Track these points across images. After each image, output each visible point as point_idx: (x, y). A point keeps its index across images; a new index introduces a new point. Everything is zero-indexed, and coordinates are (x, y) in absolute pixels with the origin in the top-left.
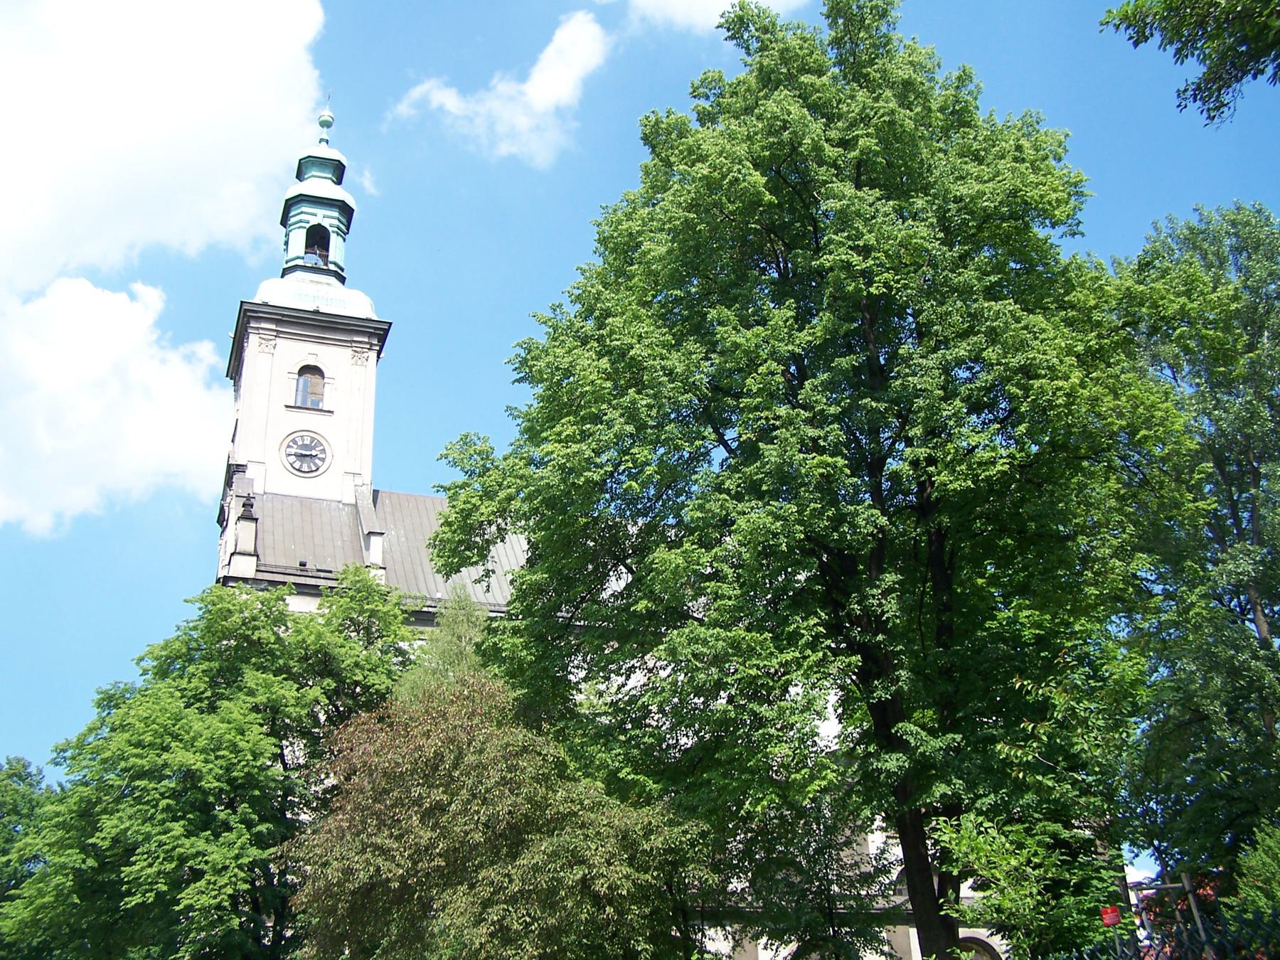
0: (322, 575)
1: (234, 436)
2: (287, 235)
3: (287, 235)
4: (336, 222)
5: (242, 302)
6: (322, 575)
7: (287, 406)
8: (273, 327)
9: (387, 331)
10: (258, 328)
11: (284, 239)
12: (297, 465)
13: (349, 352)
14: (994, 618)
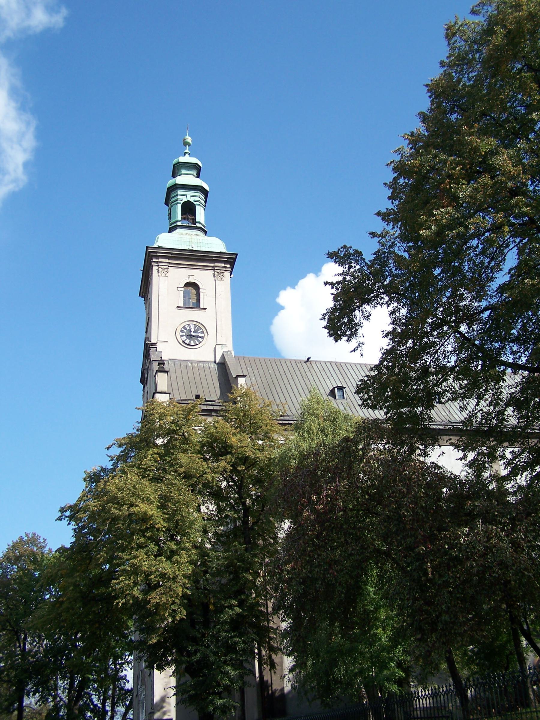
0: (210, 403)
1: (147, 329)
2: (170, 210)
3: (170, 210)
5: (147, 247)
6: (210, 403)
7: (178, 307)
8: (167, 261)
9: (235, 259)
10: (157, 262)
11: (167, 213)
12: (187, 341)
14: (429, 366)
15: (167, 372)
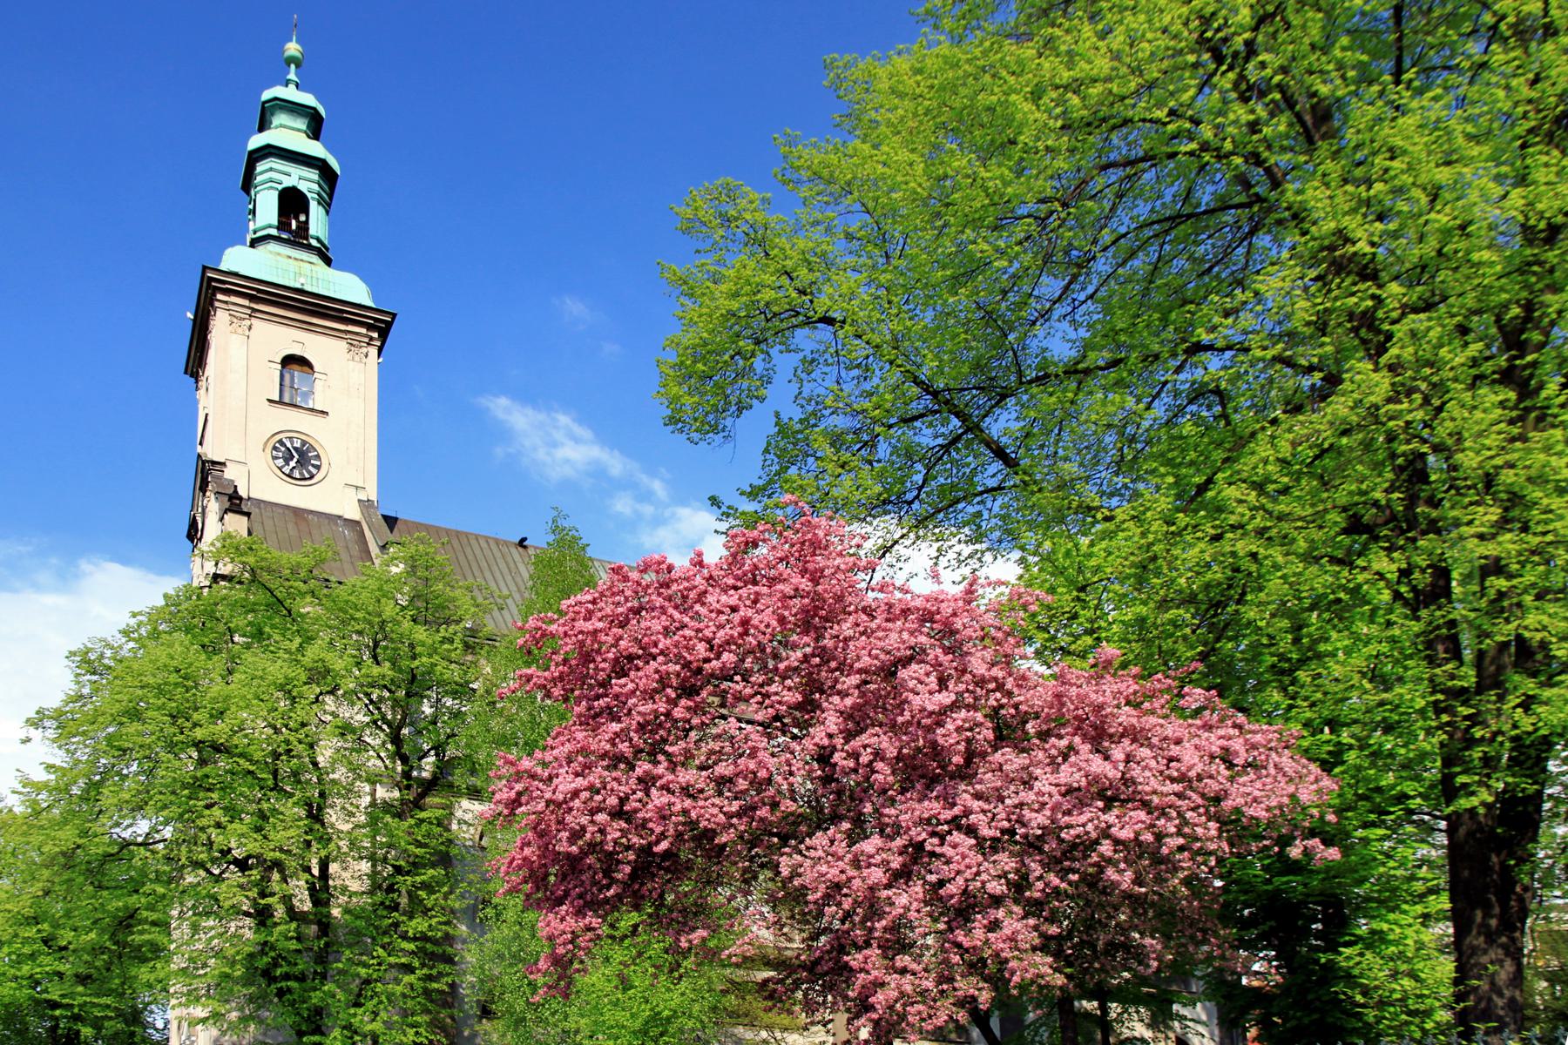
4: (316, 187)
5: (205, 268)
7: (270, 401)
9: (389, 325)
13: (343, 345)
15: (248, 514)
